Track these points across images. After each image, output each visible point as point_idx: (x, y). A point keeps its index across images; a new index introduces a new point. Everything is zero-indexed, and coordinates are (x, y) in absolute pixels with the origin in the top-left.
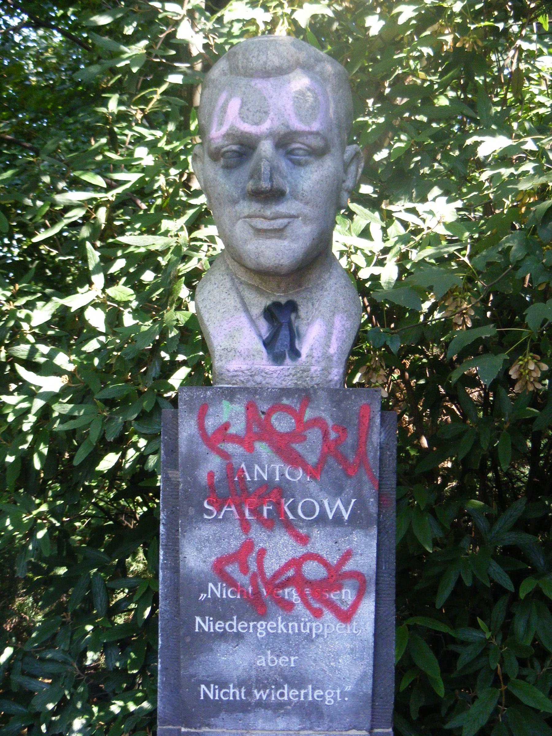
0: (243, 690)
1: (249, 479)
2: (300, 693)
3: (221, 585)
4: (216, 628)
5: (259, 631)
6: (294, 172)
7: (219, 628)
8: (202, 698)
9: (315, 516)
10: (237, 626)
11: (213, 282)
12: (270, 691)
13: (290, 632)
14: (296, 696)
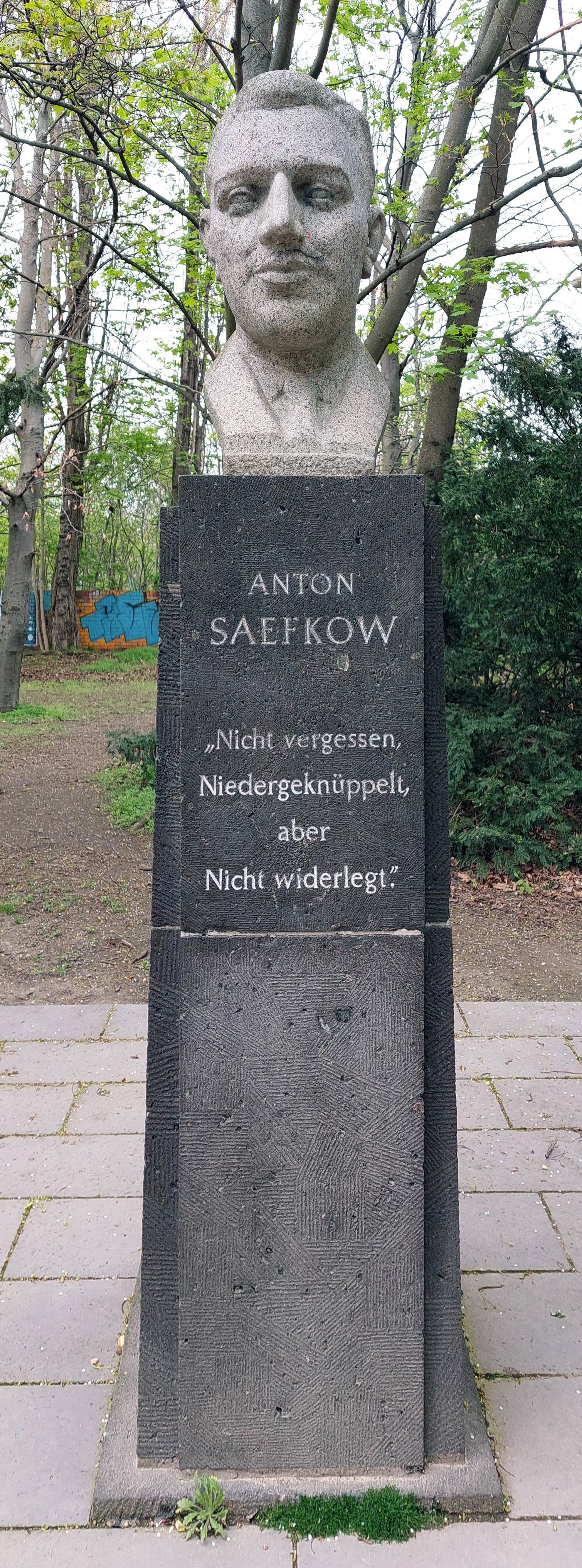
0: (261, 876)
1: (253, 643)
2: (333, 877)
3: (233, 732)
4: (227, 791)
5: (281, 793)
6: (313, 216)
7: (230, 790)
8: (208, 889)
10: (253, 787)
11: (223, 363)
12: (295, 876)
13: (320, 792)
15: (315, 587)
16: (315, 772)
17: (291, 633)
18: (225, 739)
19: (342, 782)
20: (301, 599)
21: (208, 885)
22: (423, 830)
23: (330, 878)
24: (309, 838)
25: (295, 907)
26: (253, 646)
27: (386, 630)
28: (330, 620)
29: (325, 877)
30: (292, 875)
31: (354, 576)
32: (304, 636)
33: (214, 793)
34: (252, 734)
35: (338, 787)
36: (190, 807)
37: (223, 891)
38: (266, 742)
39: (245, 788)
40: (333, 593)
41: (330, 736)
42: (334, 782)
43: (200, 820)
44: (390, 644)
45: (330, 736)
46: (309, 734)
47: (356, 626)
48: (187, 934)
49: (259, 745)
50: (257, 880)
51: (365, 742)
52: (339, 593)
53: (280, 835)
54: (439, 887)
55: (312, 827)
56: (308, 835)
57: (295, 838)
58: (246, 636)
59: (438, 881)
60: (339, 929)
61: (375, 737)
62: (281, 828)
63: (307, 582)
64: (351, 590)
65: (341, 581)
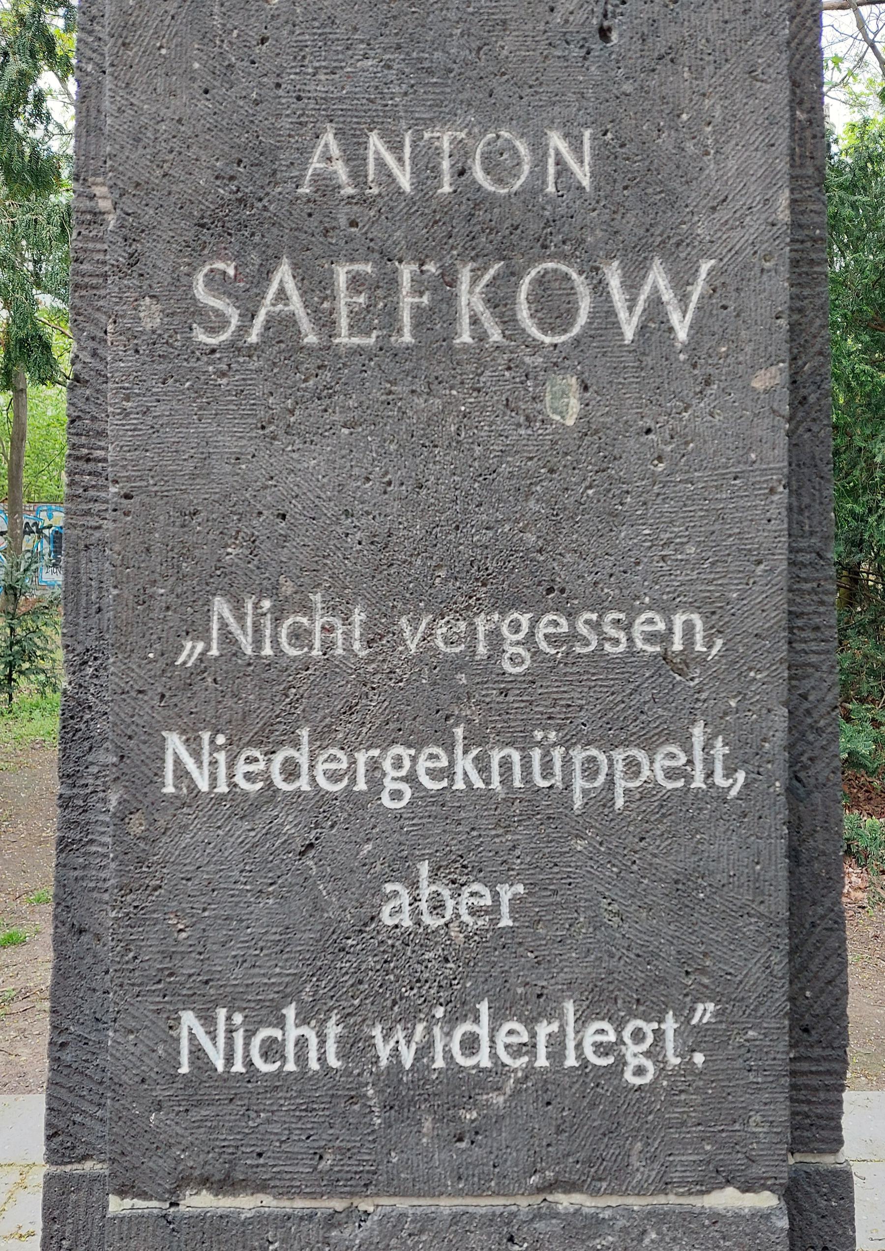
0: (333, 1030)
1: (311, 339)
2: (533, 1035)
3: (256, 606)
4: (239, 780)
5: (390, 785)
7: (248, 777)
8: (184, 1069)
9: (576, 330)
10: (312, 767)
12: (429, 1031)
13: (496, 784)
14: (516, 1051)
15: (487, 172)
16: (484, 725)
17: (417, 310)
18: (234, 627)
19: (557, 754)
20: (446, 208)
21: (185, 1058)
22: (783, 895)
23: (525, 1038)
24: (466, 918)
25: (427, 1125)
26: (310, 350)
27: (683, 299)
28: (526, 268)
29: (511, 1032)
30: (420, 1028)
31: (594, 138)
32: (452, 321)
33: (203, 785)
34: (306, 609)
35: (547, 770)
36: (137, 826)
37: (227, 1076)
38: (347, 635)
39: (291, 771)
40: (534, 190)
41: (525, 620)
42: (536, 754)
43: (164, 864)
44: (693, 346)
45: (525, 620)
46: (467, 612)
47: (600, 288)
48: (128, 1202)
49: (328, 645)
50: (322, 1042)
51: (622, 636)
52: (551, 189)
53: (386, 910)
54: (817, 1052)
55: (476, 887)
56: (463, 910)
57: (427, 919)
58: (291, 320)
59: (815, 1036)
60: (550, 1187)
61: (651, 621)
62: (389, 888)
63: (461, 152)
64: (586, 182)
65: (558, 153)
